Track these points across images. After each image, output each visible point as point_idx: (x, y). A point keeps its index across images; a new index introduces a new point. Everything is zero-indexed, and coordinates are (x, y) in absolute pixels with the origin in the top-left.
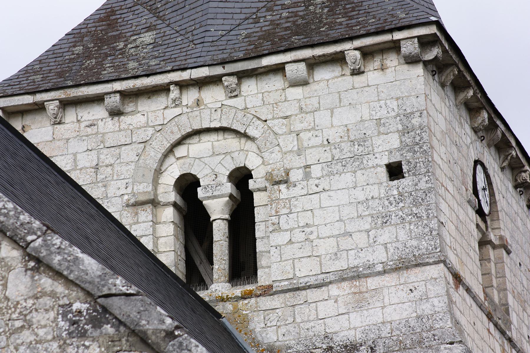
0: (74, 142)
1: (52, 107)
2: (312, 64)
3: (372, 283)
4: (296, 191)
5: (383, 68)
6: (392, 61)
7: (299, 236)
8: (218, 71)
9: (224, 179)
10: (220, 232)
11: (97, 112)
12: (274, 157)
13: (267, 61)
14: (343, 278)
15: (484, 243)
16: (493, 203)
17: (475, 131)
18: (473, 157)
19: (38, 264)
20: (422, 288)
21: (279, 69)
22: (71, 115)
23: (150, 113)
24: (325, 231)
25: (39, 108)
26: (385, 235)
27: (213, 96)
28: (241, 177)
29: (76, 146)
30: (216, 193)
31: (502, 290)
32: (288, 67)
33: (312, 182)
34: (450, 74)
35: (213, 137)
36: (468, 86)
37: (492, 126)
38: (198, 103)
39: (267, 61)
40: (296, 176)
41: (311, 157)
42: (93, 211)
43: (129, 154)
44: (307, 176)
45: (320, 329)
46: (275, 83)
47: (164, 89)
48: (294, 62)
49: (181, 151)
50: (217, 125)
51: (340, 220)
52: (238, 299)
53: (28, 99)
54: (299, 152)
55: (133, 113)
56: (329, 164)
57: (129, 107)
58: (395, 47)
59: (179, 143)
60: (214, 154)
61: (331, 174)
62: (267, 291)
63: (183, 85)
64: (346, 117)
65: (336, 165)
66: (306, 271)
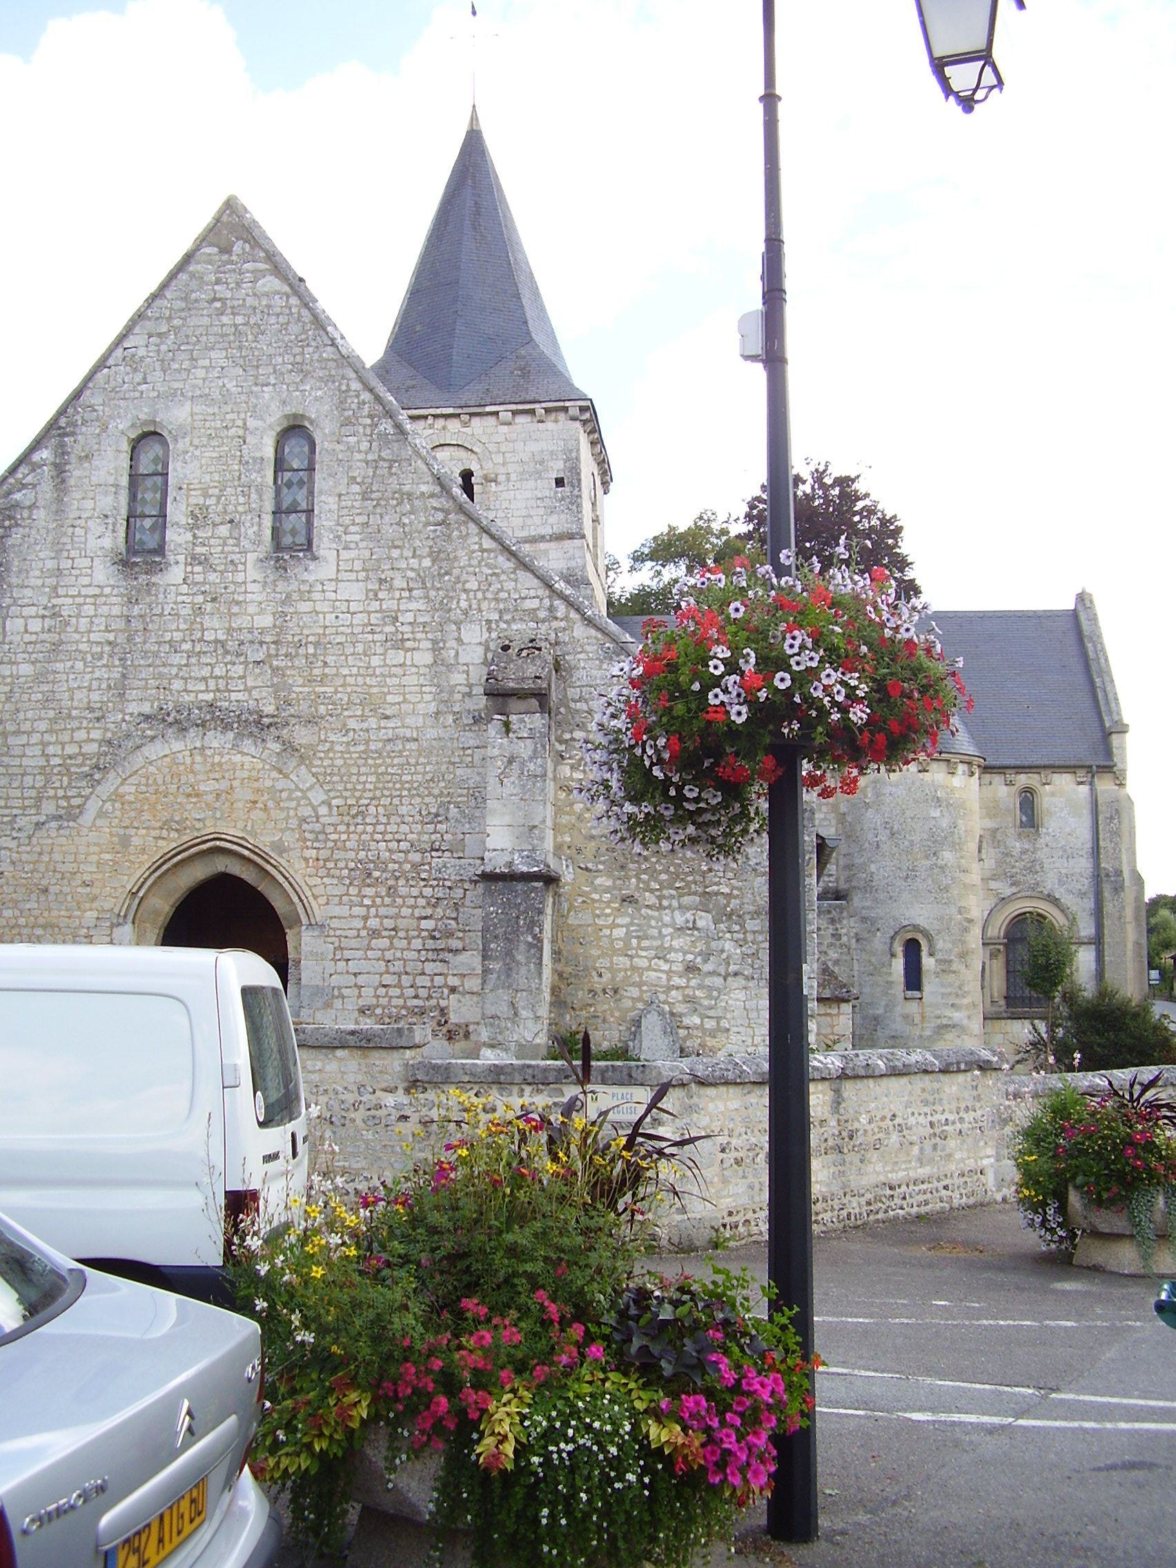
3: (543, 546)
4: (500, 488)
5: (556, 421)
6: (561, 416)
8: (459, 411)
12: (488, 466)
13: (488, 409)
26: (553, 519)
27: (454, 425)
35: (452, 448)
38: (444, 428)
39: (488, 409)
44: (508, 480)
46: (491, 420)
47: (426, 417)
48: (505, 413)
56: (522, 474)
64: (534, 447)
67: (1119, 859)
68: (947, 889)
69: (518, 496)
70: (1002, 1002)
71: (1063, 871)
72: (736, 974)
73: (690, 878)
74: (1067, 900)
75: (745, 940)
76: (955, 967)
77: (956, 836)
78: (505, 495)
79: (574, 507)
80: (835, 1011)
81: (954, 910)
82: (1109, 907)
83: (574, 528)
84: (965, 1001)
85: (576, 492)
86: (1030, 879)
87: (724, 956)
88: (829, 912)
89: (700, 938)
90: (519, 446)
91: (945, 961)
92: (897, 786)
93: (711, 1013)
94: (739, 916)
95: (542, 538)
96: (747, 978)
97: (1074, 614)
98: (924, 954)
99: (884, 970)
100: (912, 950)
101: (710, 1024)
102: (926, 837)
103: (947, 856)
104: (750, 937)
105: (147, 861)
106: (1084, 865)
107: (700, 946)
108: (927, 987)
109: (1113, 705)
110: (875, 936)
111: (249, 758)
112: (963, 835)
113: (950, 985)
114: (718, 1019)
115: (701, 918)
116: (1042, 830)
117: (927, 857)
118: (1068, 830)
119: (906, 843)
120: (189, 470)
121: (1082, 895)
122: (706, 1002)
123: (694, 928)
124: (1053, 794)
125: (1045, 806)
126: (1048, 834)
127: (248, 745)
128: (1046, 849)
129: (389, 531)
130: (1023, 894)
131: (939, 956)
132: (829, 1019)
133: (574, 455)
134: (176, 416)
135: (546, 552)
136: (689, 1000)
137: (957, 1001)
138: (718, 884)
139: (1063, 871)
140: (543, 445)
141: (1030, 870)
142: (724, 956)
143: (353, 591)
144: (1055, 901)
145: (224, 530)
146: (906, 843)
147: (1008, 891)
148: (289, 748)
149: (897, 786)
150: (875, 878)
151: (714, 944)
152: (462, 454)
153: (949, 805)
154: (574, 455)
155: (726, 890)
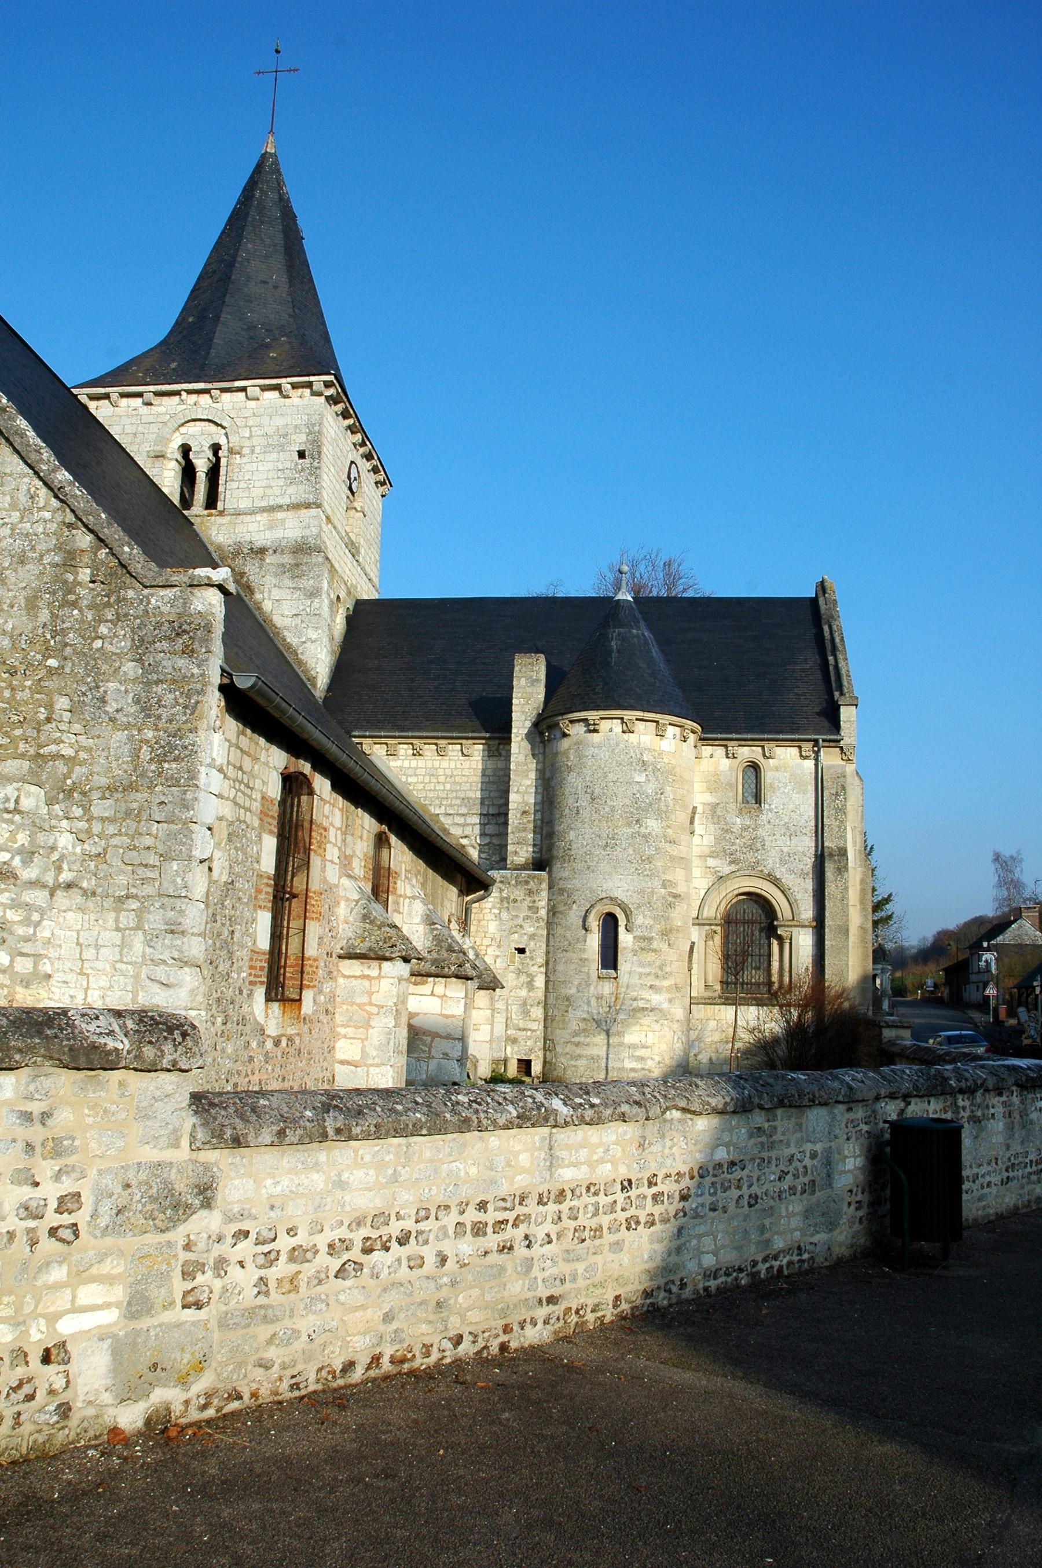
3: (280, 515)
4: (245, 460)
6: (307, 392)
7: (243, 485)
9: (206, 449)
14: (264, 510)
18: (350, 458)
20: (307, 521)
21: (243, 389)
26: (292, 490)
27: (205, 399)
28: (216, 448)
30: (604, 1065)
32: (249, 389)
33: (255, 455)
35: (203, 423)
36: (350, 417)
43: (154, 428)
44: (253, 452)
45: (248, 538)
46: (241, 395)
47: (178, 393)
49: (183, 430)
50: (205, 417)
51: (267, 479)
52: (204, 516)
55: (159, 405)
59: (183, 425)
60: (202, 434)
61: (265, 452)
62: (221, 513)
63: (189, 392)
64: (279, 421)
65: (267, 449)
66: (244, 504)
67: (844, 837)
68: (649, 860)
69: (261, 468)
70: (718, 987)
71: (785, 850)
72: (69, 886)
73: (18, 732)
74: (788, 880)
75: (89, 832)
76: (655, 945)
77: (662, 804)
78: (248, 467)
79: (313, 478)
80: (374, 972)
81: (657, 883)
82: (830, 888)
83: (311, 498)
84: (666, 983)
85: (316, 464)
86: (750, 857)
87: (55, 856)
88: (527, 883)
89: (20, 827)
90: (265, 420)
91: (644, 938)
92: (599, 747)
93: (27, 948)
94: (84, 794)
95: (280, 507)
96: (85, 893)
97: (814, 602)
98: (621, 929)
99: (579, 946)
100: (610, 923)
101: (23, 965)
102: (628, 802)
103: (652, 825)
104: (97, 828)
106: (808, 844)
107: (22, 838)
108: (623, 965)
109: (845, 683)
110: (570, 909)
112: (671, 804)
113: (650, 964)
114: (37, 957)
115: (28, 794)
116: (765, 806)
117: (629, 825)
118: (791, 807)
119: (607, 809)
121: (803, 875)
122: (21, 931)
123: (16, 811)
124: (777, 769)
125: (768, 781)
126: (771, 810)
128: (767, 826)
130: (742, 873)
131: (638, 933)
132: (366, 983)
133: (316, 428)
135: (283, 521)
137: (657, 983)
138: (58, 742)
139: (785, 850)
140: (288, 420)
141: (751, 848)
142: (55, 856)
144: (776, 882)
146: (607, 809)
147: (727, 870)
149: (599, 747)
150: (574, 846)
151: (41, 838)
152: (213, 428)
153: (655, 770)
154: (316, 428)
155: (68, 752)
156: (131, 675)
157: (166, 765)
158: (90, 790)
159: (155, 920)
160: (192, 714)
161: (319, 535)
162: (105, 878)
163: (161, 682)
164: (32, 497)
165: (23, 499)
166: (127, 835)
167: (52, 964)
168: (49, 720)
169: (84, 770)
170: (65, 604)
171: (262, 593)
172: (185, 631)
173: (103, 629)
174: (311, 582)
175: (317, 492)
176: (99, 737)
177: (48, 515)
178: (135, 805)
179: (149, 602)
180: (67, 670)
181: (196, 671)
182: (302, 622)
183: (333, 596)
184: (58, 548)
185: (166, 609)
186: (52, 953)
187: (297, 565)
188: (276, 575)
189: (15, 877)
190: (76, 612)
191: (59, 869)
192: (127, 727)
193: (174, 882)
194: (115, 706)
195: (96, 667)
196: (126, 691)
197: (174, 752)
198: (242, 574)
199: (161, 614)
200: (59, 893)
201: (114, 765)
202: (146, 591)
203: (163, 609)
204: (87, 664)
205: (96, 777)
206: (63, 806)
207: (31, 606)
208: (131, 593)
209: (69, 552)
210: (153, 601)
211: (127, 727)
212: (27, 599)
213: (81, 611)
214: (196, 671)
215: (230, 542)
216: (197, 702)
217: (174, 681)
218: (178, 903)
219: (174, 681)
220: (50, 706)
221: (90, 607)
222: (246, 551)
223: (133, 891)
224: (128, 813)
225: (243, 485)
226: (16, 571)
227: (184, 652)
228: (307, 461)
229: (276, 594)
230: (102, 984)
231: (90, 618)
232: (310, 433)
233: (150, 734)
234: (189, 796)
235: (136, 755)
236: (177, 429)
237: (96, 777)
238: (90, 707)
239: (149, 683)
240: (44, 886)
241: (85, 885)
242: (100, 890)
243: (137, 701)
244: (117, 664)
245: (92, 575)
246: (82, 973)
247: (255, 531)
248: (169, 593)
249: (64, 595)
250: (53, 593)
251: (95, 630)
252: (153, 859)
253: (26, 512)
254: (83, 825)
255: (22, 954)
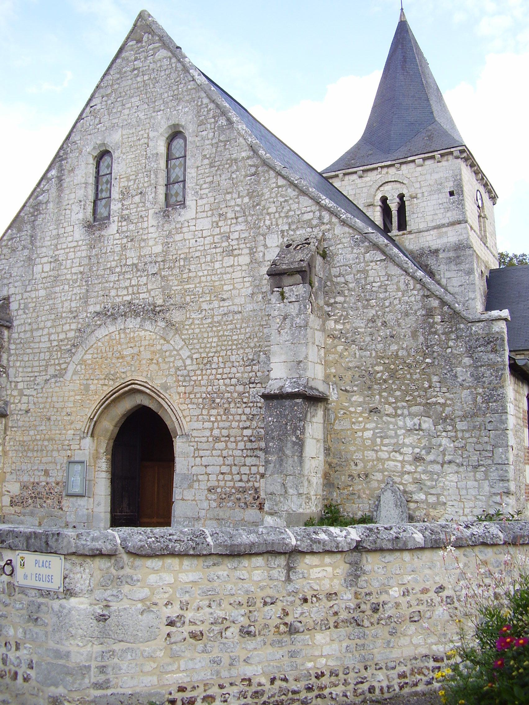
0: (347, 185)
1: (341, 176)
2: (424, 159)
3: (444, 230)
4: (419, 201)
5: (447, 160)
6: (450, 157)
8: (394, 162)
10: (395, 213)
11: (355, 177)
13: (409, 159)
14: (434, 228)
15: (480, 216)
16: (482, 203)
17: (477, 180)
19: (344, 223)
20: (460, 231)
22: (347, 178)
23: (372, 177)
24: (429, 213)
25: (337, 176)
26: (449, 214)
27: (392, 170)
29: (348, 188)
31: (485, 231)
34: (469, 162)
35: (392, 183)
37: (483, 179)
38: (387, 173)
39: (409, 159)
40: (419, 196)
41: (424, 190)
42: (355, 208)
43: (365, 190)
44: (423, 196)
45: (427, 245)
46: (412, 165)
47: (376, 169)
49: (382, 189)
53: (334, 173)
54: (420, 188)
56: (430, 192)
57: (365, 175)
58: (451, 153)
59: (381, 186)
62: (410, 233)
63: (382, 167)
64: (436, 176)
65: (431, 193)
66: (422, 226)
72: (450, 462)
75: (456, 437)
78: (422, 205)
79: (460, 206)
83: (461, 218)
85: (461, 198)
87: (441, 449)
90: (428, 177)
93: (433, 491)
94: (452, 420)
95: (443, 226)
101: (432, 499)
104: (460, 435)
105: (98, 398)
107: (424, 442)
111: (148, 332)
114: (438, 495)
115: (425, 422)
120: (121, 167)
122: (429, 483)
123: (420, 429)
127: (148, 325)
129: (225, 184)
133: (458, 177)
134: (114, 139)
135: (446, 232)
136: (417, 482)
138: (436, 396)
140: (441, 175)
142: (441, 449)
143: (205, 224)
145: (137, 199)
148: (170, 324)
151: (434, 441)
152: (398, 185)
154: (458, 177)
155: (441, 401)
156: (468, 364)
157: (490, 404)
158: (455, 418)
159: (494, 475)
160: (500, 379)
161: (468, 238)
162: (467, 457)
163: (483, 366)
164: (407, 285)
165: (402, 286)
166: (475, 437)
167: (446, 498)
168: (430, 387)
169: (450, 409)
170: (430, 333)
171: (440, 275)
172: (491, 341)
173: (451, 343)
174: (467, 266)
175: (464, 213)
176: (456, 393)
177: (416, 292)
178: (477, 423)
179: (472, 329)
180: (436, 363)
181: (499, 359)
182: (465, 289)
183: (480, 271)
184: (424, 307)
185: (480, 332)
186: (445, 493)
187: (458, 257)
188: (446, 264)
189: (424, 459)
190: (436, 336)
191: (444, 455)
192: (469, 388)
193: (501, 458)
194: (462, 378)
195: (450, 361)
196: (466, 371)
197: (494, 399)
198: (427, 266)
199: (479, 334)
200: (445, 466)
201: (465, 405)
202: (470, 324)
203: (479, 332)
204: (445, 360)
205: (456, 412)
206: (442, 426)
207: (414, 334)
208: (462, 326)
209: (429, 309)
210: (474, 328)
211: (469, 388)
212: (411, 332)
213: (439, 335)
214: (499, 359)
215: (417, 248)
216: (502, 374)
217: (489, 365)
218: (504, 467)
219: (489, 365)
220: (430, 381)
221: (443, 334)
222: (427, 252)
223: (482, 462)
224: (474, 427)
225: (420, 215)
226: (404, 319)
227: (492, 351)
228: (456, 197)
229: (448, 275)
230: (471, 505)
231: (444, 338)
232: (455, 180)
233: (481, 390)
234: (504, 417)
235: (475, 400)
236: (378, 188)
237: (456, 412)
238: (449, 381)
239: (477, 367)
240: (438, 463)
241: (457, 461)
242: (465, 463)
243: (472, 375)
244: (460, 359)
245: (442, 319)
246: (460, 501)
247: (431, 240)
248: (481, 324)
249: (430, 329)
250: (424, 329)
251: (447, 344)
252: (489, 448)
253: (404, 293)
254: (453, 434)
255: (431, 494)
